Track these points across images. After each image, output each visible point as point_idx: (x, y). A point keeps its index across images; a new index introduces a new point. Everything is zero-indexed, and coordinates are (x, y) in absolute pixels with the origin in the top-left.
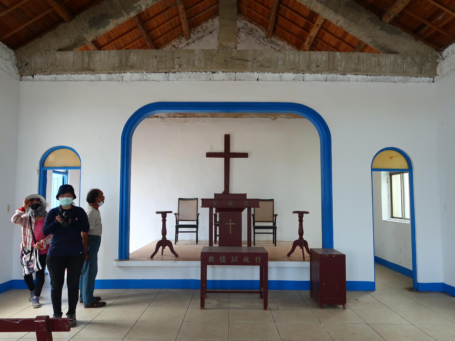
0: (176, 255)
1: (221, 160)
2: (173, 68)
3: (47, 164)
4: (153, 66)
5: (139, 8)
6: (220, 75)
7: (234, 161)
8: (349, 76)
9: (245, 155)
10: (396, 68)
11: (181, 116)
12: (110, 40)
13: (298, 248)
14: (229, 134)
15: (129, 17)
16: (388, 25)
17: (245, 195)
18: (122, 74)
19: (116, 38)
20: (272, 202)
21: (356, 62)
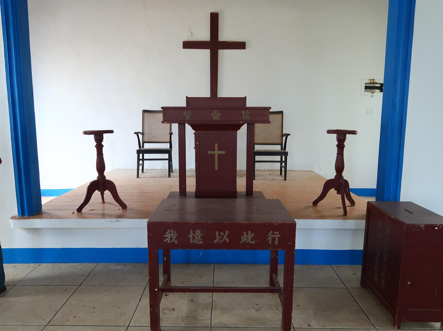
0: (124, 206)
1: (206, 53)
7: (225, 55)
9: (241, 45)
13: (333, 192)
14: (217, 12)
17: (244, 99)
20: (280, 115)
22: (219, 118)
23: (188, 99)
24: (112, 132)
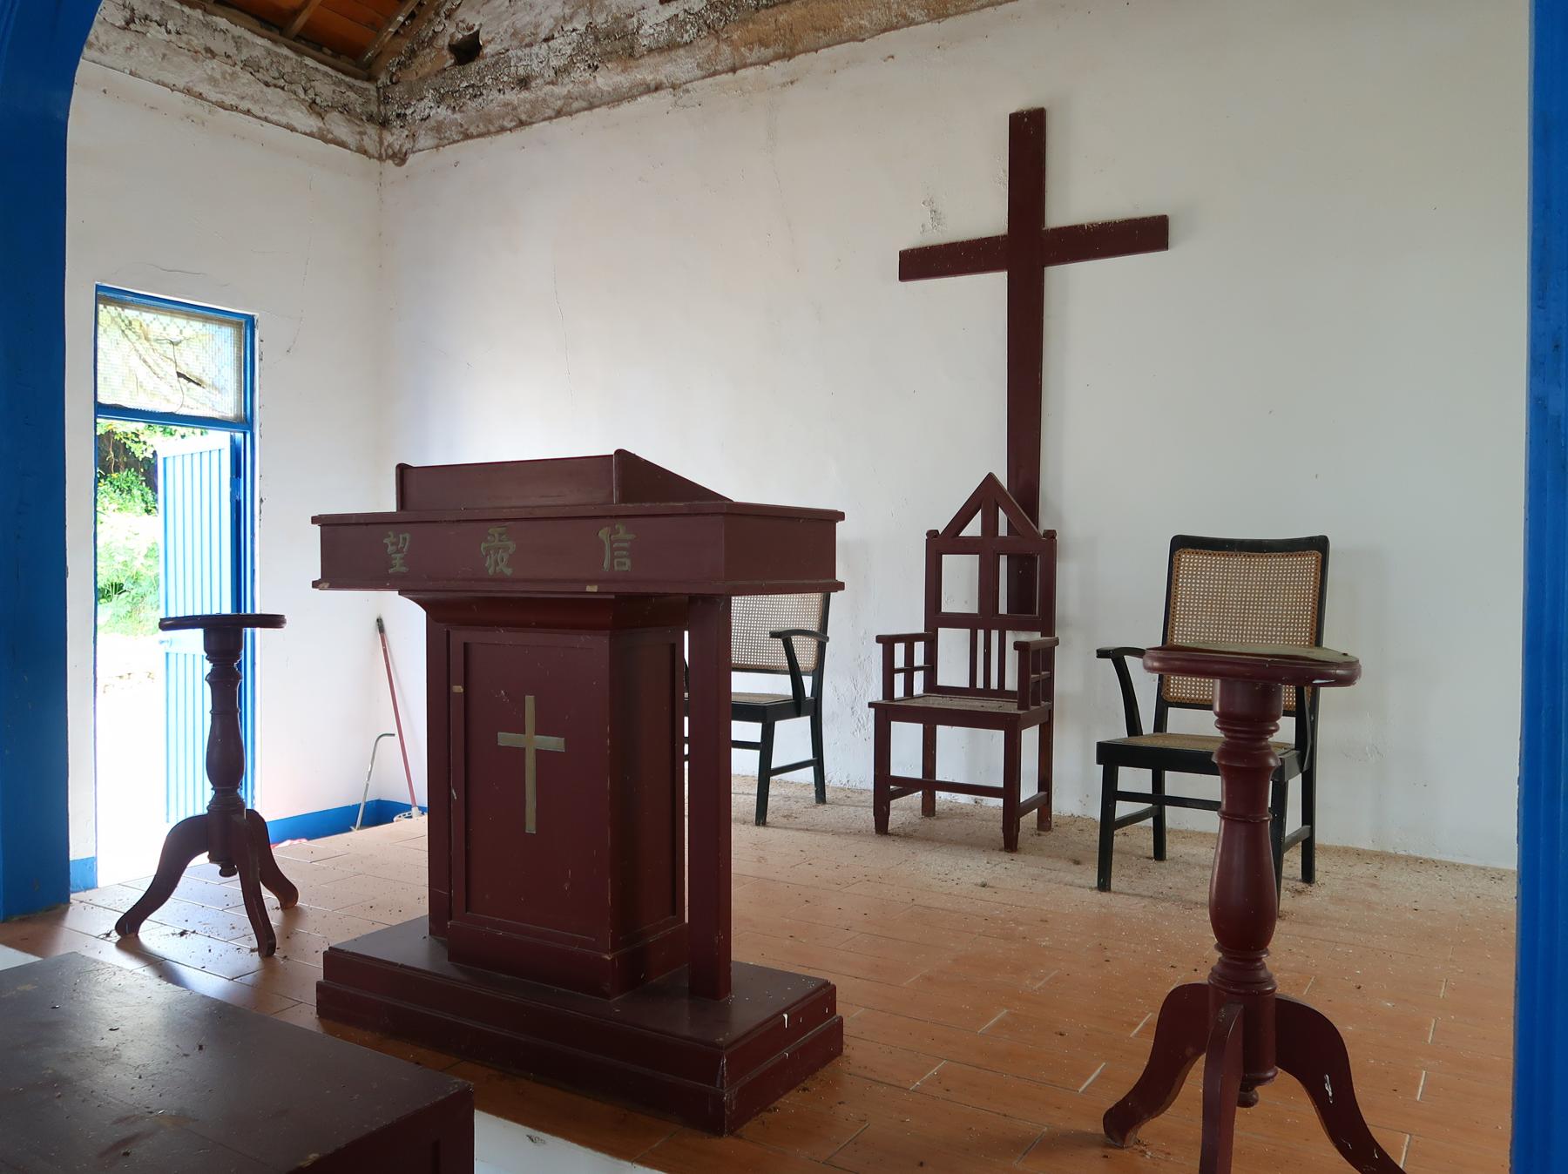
9: (1147, 234)
11: (769, 52)
22: (508, 566)
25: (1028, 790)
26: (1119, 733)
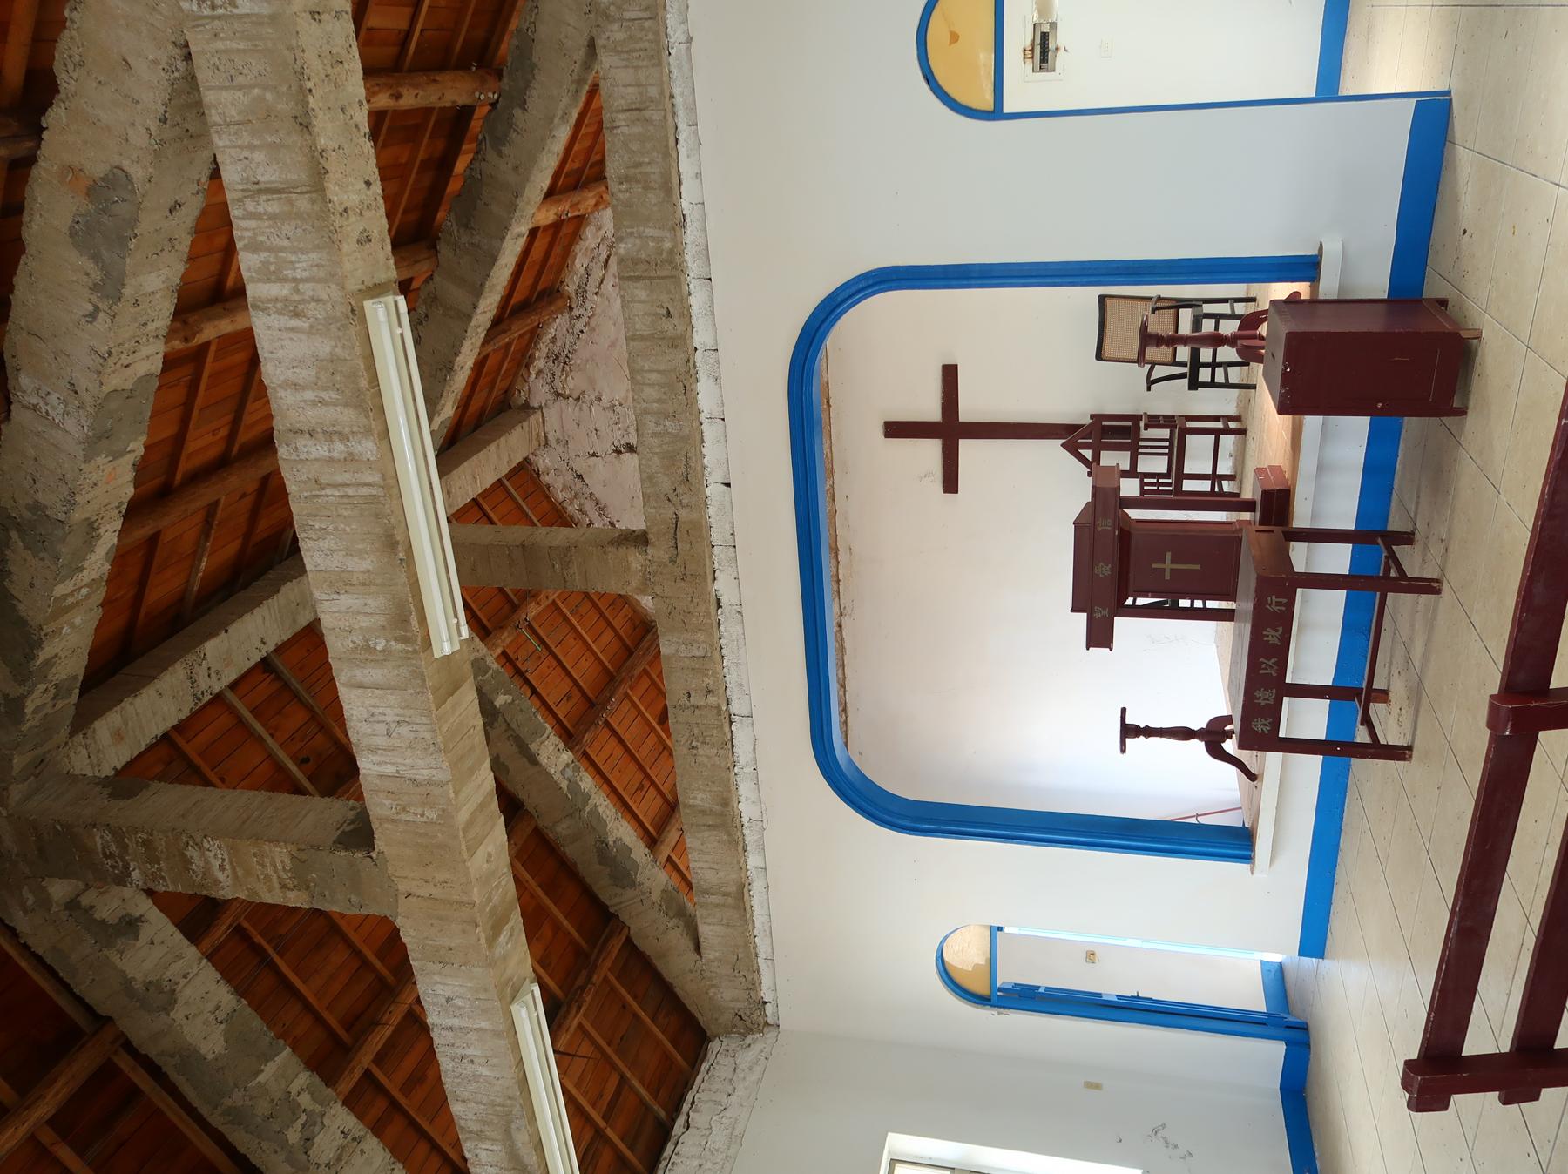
1: (966, 447)
2: (718, 708)
3: (982, 988)
4: (717, 755)
5: (569, 773)
6: (723, 585)
8: (685, 204)
9: (950, 374)
10: (641, 45)
12: (647, 784)
15: (594, 790)
16: (505, 80)
18: (745, 820)
19: (640, 767)
20: (1109, 302)
21: (638, 188)
23: (1075, 609)
24: (1124, 711)
25: (1219, 425)
26: (1186, 381)
